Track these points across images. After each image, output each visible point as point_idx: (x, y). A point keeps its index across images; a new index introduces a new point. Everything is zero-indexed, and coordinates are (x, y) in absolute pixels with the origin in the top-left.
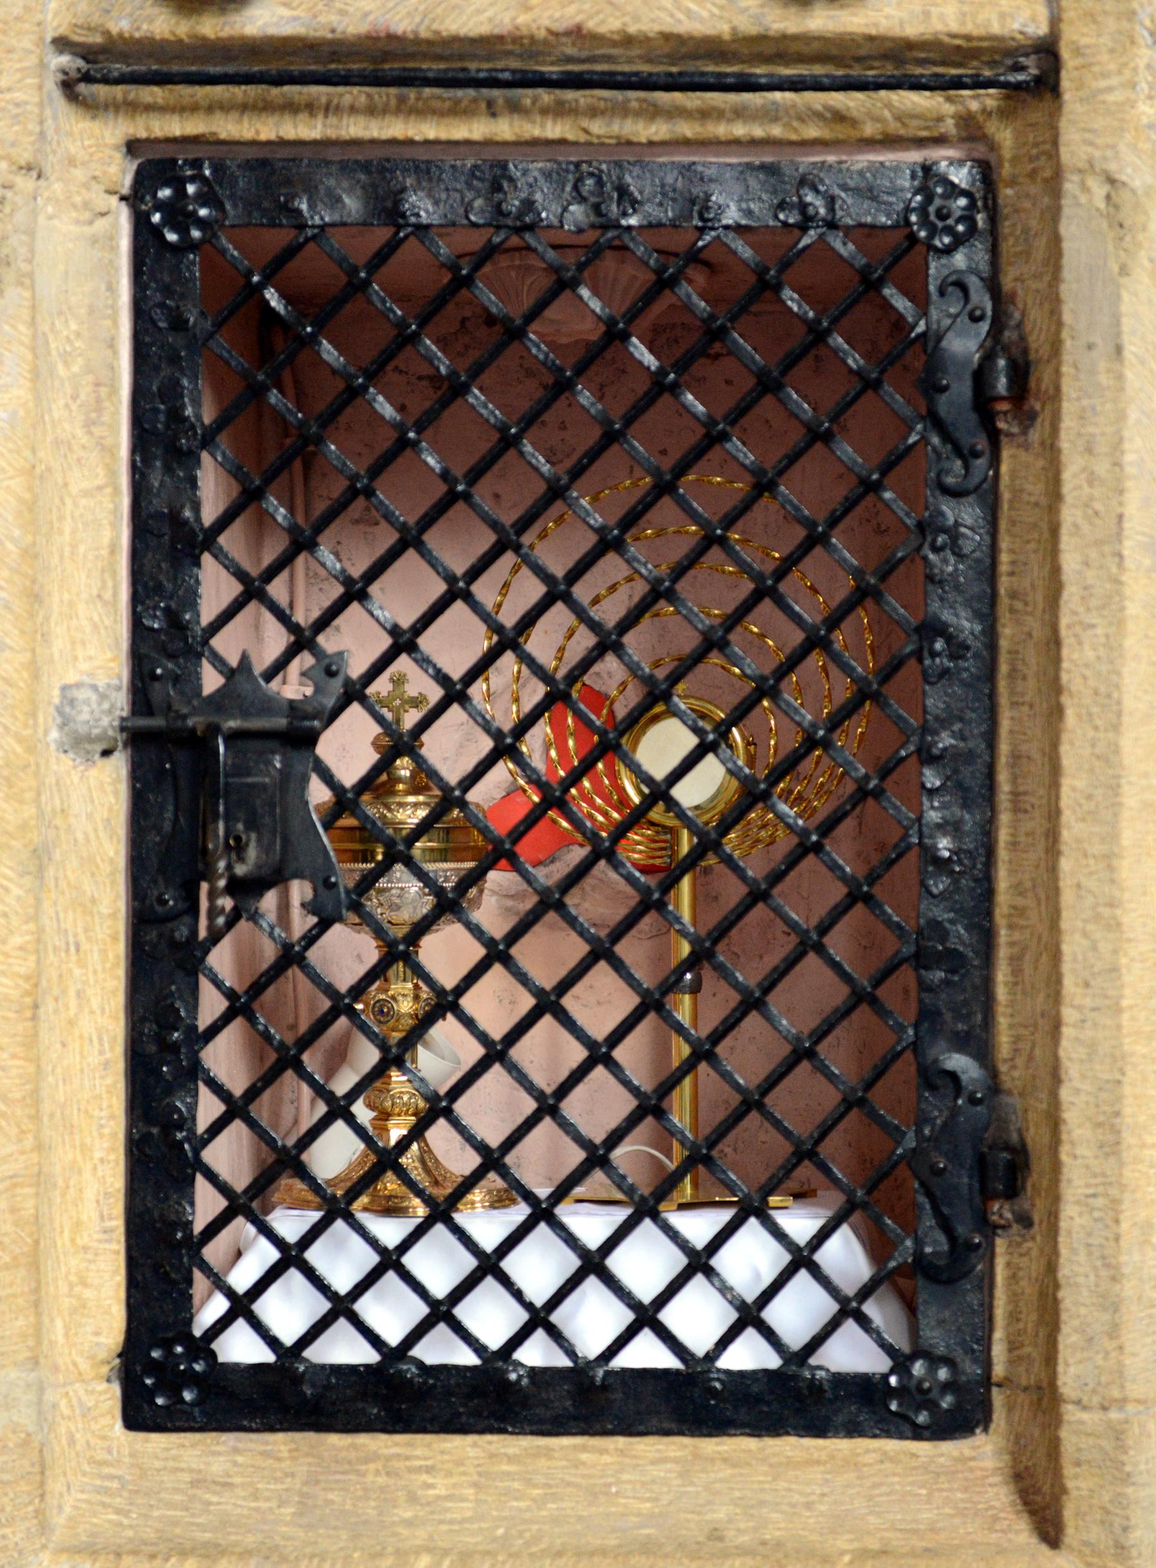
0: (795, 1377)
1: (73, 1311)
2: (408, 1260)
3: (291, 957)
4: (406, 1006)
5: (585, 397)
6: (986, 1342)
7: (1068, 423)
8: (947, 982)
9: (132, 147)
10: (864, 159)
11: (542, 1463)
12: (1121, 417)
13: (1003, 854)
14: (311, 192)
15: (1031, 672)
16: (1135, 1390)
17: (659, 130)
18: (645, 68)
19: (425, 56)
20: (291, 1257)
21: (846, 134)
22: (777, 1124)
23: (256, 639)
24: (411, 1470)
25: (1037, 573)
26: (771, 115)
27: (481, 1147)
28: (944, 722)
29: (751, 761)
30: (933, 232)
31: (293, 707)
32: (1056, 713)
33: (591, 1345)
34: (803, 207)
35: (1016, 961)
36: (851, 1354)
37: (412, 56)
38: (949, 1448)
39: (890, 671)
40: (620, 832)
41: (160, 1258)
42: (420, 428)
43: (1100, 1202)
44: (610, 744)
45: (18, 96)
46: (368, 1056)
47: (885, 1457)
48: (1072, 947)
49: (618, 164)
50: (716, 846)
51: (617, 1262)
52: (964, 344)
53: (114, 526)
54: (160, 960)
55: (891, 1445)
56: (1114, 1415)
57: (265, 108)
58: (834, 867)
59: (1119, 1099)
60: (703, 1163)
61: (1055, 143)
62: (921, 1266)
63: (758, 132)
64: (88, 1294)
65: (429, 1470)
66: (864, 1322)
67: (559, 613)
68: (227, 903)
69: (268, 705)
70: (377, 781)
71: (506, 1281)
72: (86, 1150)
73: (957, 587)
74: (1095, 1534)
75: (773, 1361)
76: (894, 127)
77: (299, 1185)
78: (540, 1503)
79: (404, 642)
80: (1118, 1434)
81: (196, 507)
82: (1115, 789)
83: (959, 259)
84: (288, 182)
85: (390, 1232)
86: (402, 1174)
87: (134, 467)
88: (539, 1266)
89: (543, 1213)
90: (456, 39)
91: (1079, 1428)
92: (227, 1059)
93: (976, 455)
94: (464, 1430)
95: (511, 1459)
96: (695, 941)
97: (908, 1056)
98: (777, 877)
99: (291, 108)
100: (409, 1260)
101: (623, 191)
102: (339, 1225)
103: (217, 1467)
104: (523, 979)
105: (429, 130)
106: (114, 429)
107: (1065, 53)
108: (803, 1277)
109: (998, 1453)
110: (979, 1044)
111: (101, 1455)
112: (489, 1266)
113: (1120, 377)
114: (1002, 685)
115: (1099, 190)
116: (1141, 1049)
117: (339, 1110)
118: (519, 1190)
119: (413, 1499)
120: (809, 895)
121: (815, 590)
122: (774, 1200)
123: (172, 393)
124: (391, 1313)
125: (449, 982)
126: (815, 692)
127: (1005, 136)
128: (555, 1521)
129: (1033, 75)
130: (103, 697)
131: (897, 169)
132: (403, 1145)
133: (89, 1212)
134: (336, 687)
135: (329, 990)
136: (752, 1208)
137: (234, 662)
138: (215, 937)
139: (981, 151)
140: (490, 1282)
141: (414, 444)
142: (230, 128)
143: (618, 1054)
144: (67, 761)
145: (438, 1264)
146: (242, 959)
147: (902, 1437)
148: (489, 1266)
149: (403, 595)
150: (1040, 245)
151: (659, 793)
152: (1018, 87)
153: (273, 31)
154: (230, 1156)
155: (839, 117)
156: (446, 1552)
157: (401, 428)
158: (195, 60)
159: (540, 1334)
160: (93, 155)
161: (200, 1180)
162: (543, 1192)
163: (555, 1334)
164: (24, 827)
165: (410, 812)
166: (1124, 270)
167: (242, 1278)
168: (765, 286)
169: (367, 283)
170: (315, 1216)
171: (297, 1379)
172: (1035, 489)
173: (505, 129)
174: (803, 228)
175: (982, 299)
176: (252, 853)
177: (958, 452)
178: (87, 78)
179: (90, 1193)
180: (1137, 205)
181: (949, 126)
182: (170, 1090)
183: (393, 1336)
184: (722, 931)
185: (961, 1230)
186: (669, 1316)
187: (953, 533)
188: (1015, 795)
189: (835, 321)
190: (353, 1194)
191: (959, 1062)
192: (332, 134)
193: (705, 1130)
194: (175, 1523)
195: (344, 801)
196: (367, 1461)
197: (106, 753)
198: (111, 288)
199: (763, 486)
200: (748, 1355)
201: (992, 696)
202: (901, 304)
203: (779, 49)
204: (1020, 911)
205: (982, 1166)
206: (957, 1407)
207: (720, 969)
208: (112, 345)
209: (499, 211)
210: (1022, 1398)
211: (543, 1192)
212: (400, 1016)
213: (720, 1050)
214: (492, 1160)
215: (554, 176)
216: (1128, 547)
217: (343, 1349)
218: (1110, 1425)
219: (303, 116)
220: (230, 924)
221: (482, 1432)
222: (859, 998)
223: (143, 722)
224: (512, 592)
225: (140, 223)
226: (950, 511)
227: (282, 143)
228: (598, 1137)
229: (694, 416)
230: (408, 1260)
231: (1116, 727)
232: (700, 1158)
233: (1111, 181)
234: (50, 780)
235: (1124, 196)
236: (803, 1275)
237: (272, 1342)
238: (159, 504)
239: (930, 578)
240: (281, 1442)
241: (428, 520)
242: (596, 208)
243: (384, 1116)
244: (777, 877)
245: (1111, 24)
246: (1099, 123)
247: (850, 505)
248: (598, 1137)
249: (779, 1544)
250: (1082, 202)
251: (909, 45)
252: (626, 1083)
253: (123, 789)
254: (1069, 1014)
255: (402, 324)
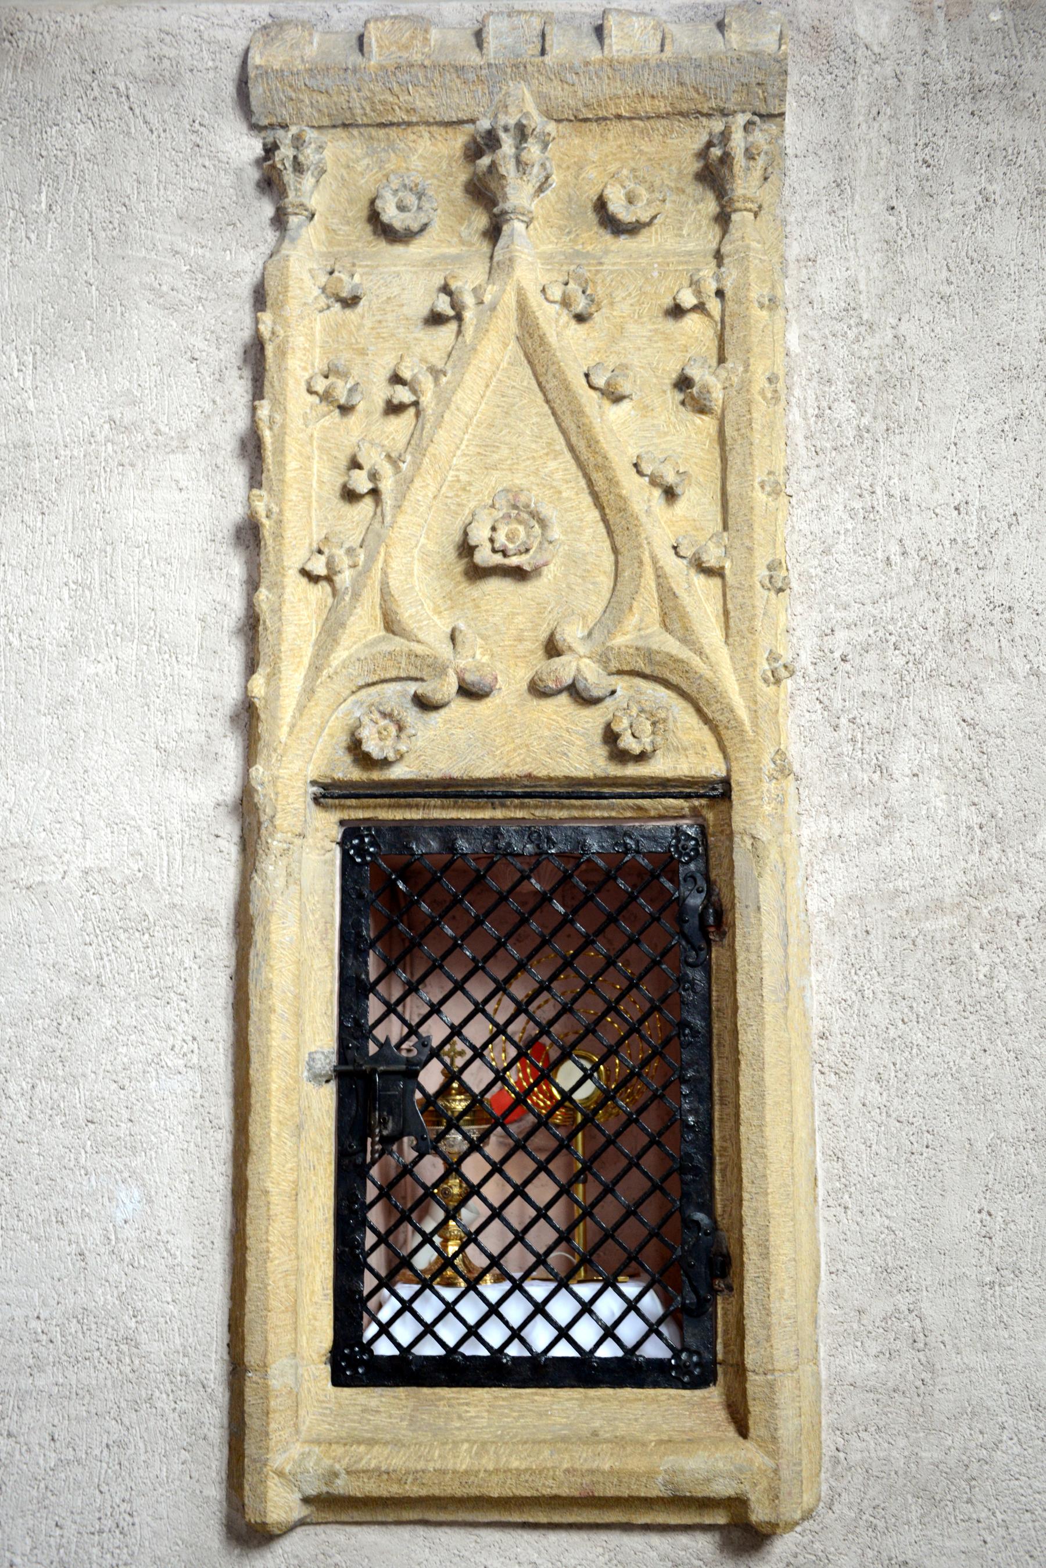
0: (630, 1360)
1: (310, 1331)
2: (458, 1307)
3: (407, 1170)
4: (456, 1191)
5: (534, 925)
6: (714, 1344)
7: (739, 938)
8: (694, 1181)
9: (342, 823)
10: (650, 825)
11: (518, 1400)
12: (761, 936)
13: (717, 1123)
14: (417, 840)
15: (727, 1044)
16: (778, 1365)
17: (564, 814)
18: (557, 790)
19: (465, 786)
20: (406, 1306)
21: (643, 814)
22: (620, 1244)
23: (393, 1030)
24: (459, 1404)
25: (728, 1000)
26: (611, 808)
27: (489, 1256)
28: (690, 1065)
29: (608, 1078)
30: (681, 855)
31: (408, 1061)
32: (737, 1063)
33: (539, 1346)
34: (625, 844)
35: (723, 1171)
36: (654, 1350)
37: (458, 786)
38: (699, 1393)
39: (666, 1042)
40: (551, 1113)
41: (349, 1308)
42: (463, 938)
43: (761, 1280)
44: (546, 1075)
45: (296, 806)
46: (440, 1215)
47: (670, 1397)
48: (746, 1165)
49: (547, 827)
50: (592, 1120)
51: (550, 1308)
52: (696, 901)
53: (332, 983)
54: (349, 1172)
55: (673, 1392)
56: (769, 1377)
57: (399, 806)
58: (643, 1129)
59: (768, 1233)
60: (589, 1258)
61: (730, 819)
62: (685, 1309)
63: (606, 814)
64: (317, 1324)
65: (467, 1404)
66: (660, 1335)
67: (523, 1018)
68: (378, 1147)
69: (397, 1060)
70: (444, 1090)
71: (501, 1317)
72: (316, 1258)
73: (695, 1006)
74: (763, 1432)
75: (620, 1353)
76: (663, 812)
77: (409, 1273)
78: (517, 1419)
79: (456, 1031)
80: (771, 1386)
81: (367, 974)
82: (763, 1096)
83: (692, 866)
84: (407, 836)
85: (450, 1294)
86: (455, 1268)
87: (341, 957)
88: (516, 1310)
89: (517, 1286)
90: (479, 779)
91: (754, 1383)
92: (376, 1216)
93: (701, 949)
94: (483, 1386)
95: (503, 1399)
96: (583, 1162)
97: (677, 1214)
98: (618, 1134)
99: (409, 807)
100: (459, 1308)
101: (549, 839)
102: (428, 1292)
103: (374, 1403)
104: (508, 1180)
105: (467, 815)
106: (332, 941)
107: (733, 785)
108: (632, 1314)
109: (720, 1395)
110: (708, 1208)
111: (322, 1398)
112: (494, 1310)
113: (760, 920)
114: (715, 1049)
115: (749, 841)
116: (776, 1211)
117: (427, 1239)
118: (505, 1275)
119: (460, 1417)
120: (632, 1142)
121: (632, 1008)
122: (621, 1278)
123: (357, 925)
124: (450, 1332)
125: (476, 1181)
126: (634, 1052)
127: (710, 816)
128: (523, 1427)
129: (720, 792)
130: (327, 1057)
131: (665, 828)
132: (456, 1255)
133: (318, 1287)
134: (427, 1051)
135: (423, 1185)
136: (610, 1283)
137: (382, 1040)
138: (374, 1162)
139: (700, 821)
140: (494, 1317)
141: (461, 946)
142: (384, 815)
143: (550, 1213)
144: (311, 1085)
145: (471, 1310)
146: (384, 1173)
147: (677, 1388)
148: (494, 1310)
149: (456, 1010)
150: (726, 861)
151: (567, 1096)
152: (714, 797)
153: (402, 777)
154: (377, 1260)
155: (640, 808)
156: (475, 1442)
157: (455, 939)
158: (369, 788)
159: (516, 1341)
160: (327, 826)
161: (367, 1273)
162: (517, 1275)
163: (523, 1341)
164: (293, 1116)
165: (459, 1104)
166: (760, 875)
167: (384, 1316)
168: (609, 877)
169: (441, 878)
170: (417, 1287)
171: (409, 1362)
172: (726, 964)
173: (499, 814)
174: (625, 853)
175: (701, 883)
176: (390, 1125)
177: (693, 948)
178: (324, 796)
179: (318, 1279)
180: (765, 848)
181: (687, 811)
182: (353, 1232)
183: (451, 1342)
184: (596, 1156)
185: (702, 1292)
186: (574, 1333)
187: (692, 983)
188: (721, 1097)
189: (639, 892)
190: (434, 1277)
191: (700, 1216)
192: (426, 816)
193: (591, 1245)
194: (355, 1429)
195: (430, 1101)
196: (440, 1400)
197: (327, 1081)
198: (332, 882)
199: (610, 962)
200: (608, 1351)
201: (711, 1054)
202: (668, 885)
203: (615, 782)
204: (725, 1149)
205: (710, 1263)
206: (702, 1374)
207: (594, 1174)
208: (332, 906)
209: (496, 847)
210: (730, 1369)
211: (517, 1275)
212: (453, 1195)
213: (595, 1211)
214: (495, 1261)
215: (520, 833)
216: (765, 992)
217: (429, 1349)
218: (767, 1381)
219: (414, 810)
220: (380, 1157)
221: (490, 1387)
222: (655, 1187)
223: (344, 1068)
224: (502, 1009)
225: (345, 854)
226: (689, 972)
227: (405, 820)
228: (541, 1251)
229: (580, 933)
230: (458, 1307)
231: (762, 1069)
232: (586, 1260)
233: (754, 838)
234: (304, 1094)
235: (759, 844)
236: (633, 1314)
237: (398, 1345)
238: (351, 973)
239: (683, 1002)
240: (401, 1392)
241: (467, 978)
242: (538, 846)
243: (446, 1240)
244: (618, 1134)
245: (752, 773)
246: (748, 814)
247: (647, 971)
248: (541, 1251)
249: (623, 1438)
250: (742, 847)
251: (668, 780)
252: (554, 1227)
253: (334, 1096)
254: (746, 1196)
255: (455, 895)
